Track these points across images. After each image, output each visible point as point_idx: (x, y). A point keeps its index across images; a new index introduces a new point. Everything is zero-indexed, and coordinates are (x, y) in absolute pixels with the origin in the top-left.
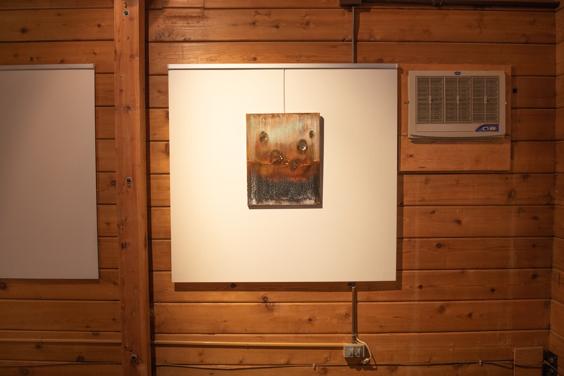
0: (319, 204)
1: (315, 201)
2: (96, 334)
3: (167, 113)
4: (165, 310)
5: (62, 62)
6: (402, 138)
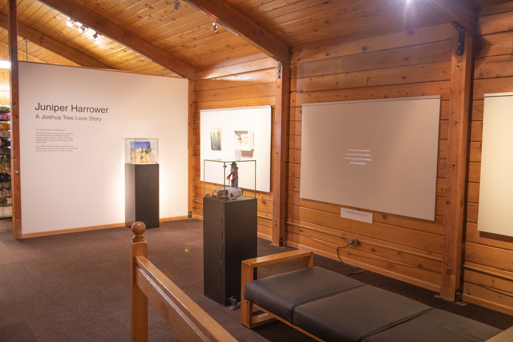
2: (430, 253)
3: (482, 123)
4: (473, 248)
5: (423, 95)
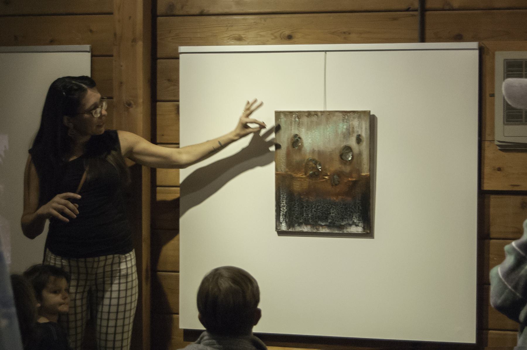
0: (368, 232)
1: (364, 228)
6: (486, 144)
